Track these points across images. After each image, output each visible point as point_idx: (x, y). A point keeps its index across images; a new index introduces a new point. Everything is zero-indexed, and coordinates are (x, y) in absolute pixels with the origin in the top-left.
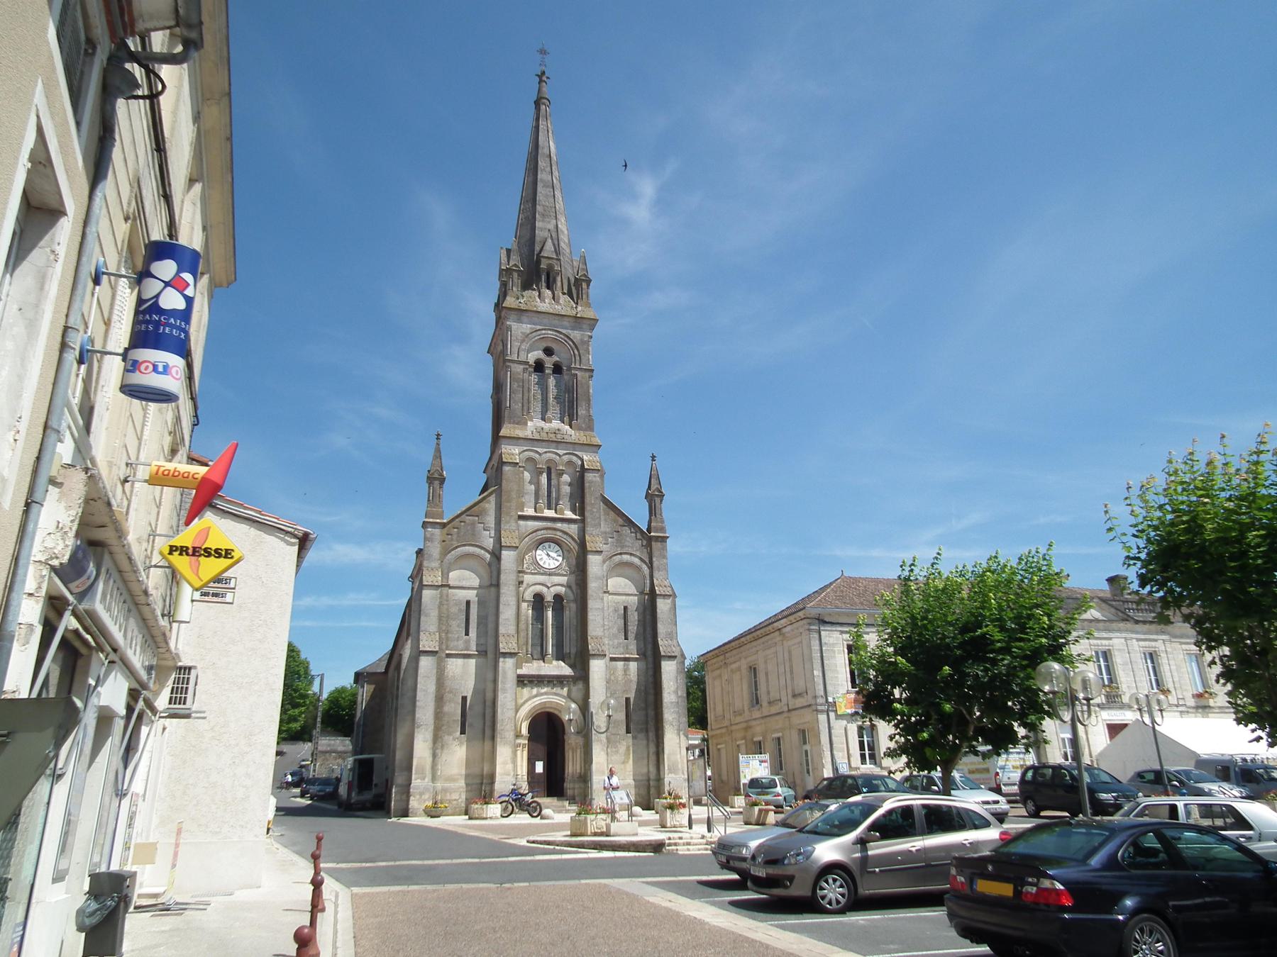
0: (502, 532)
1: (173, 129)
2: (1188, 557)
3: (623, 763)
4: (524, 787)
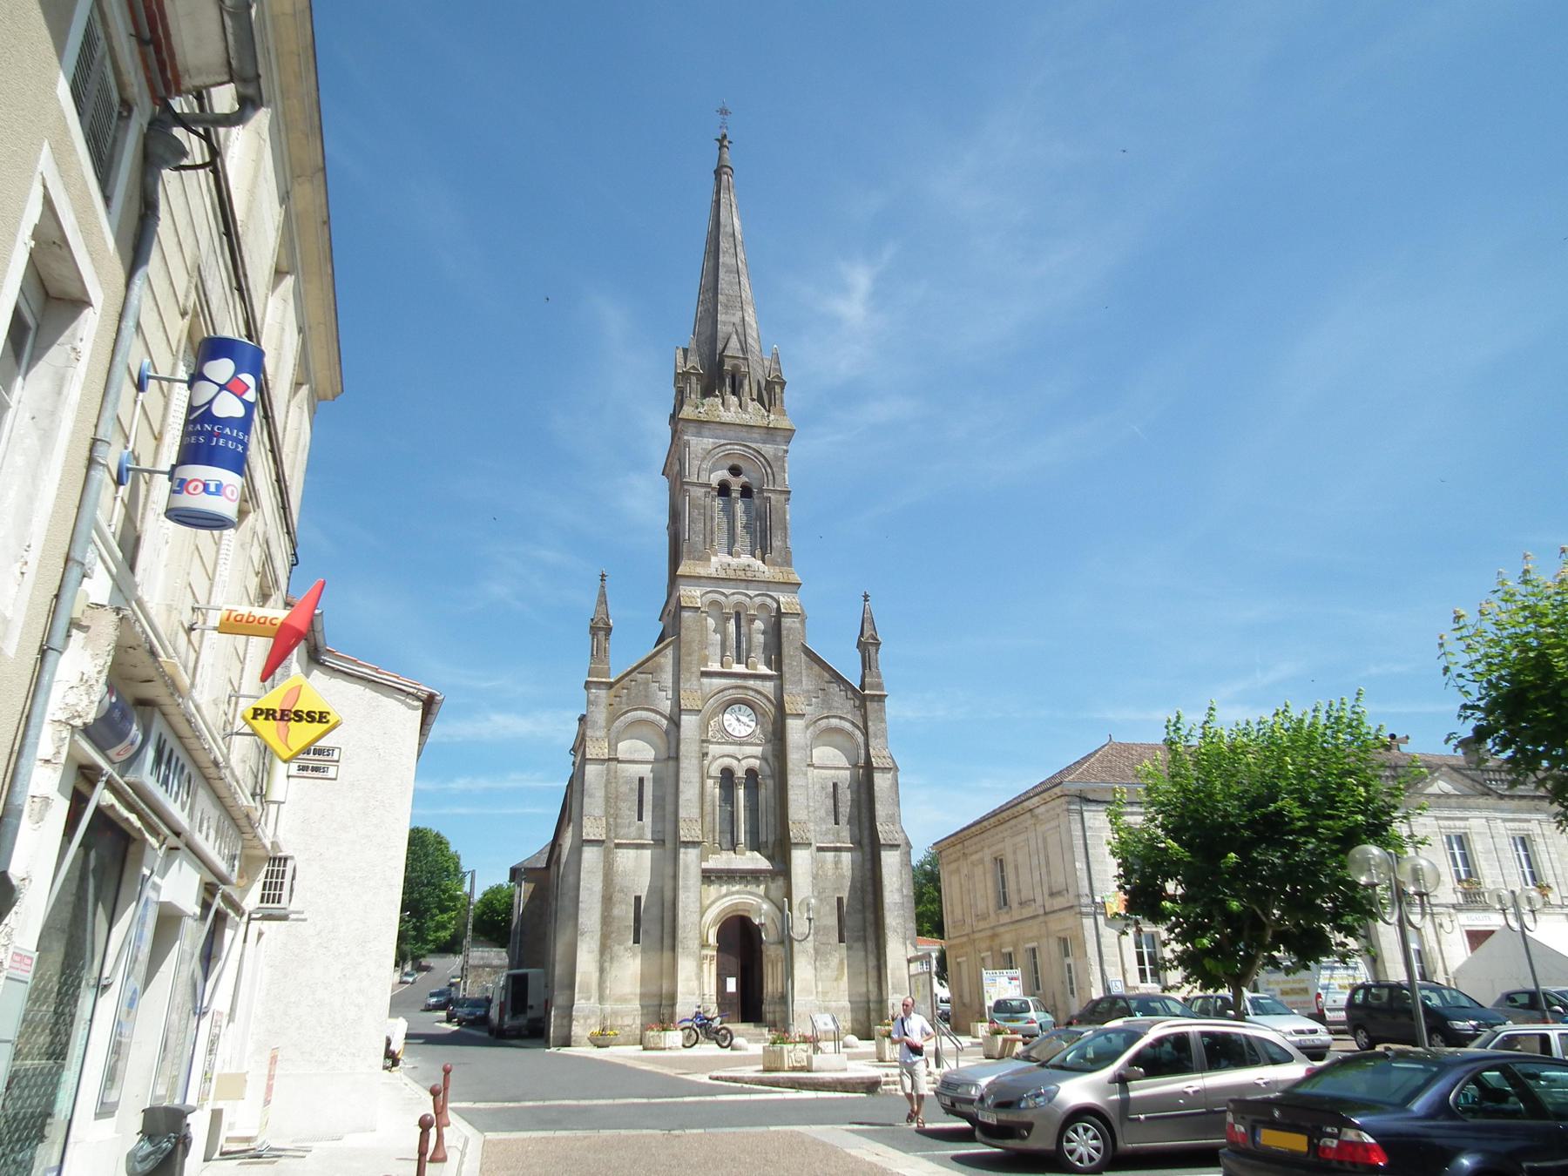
0: (682, 692)
1: (249, 210)
2: (1534, 704)
3: (836, 979)
4: (713, 1010)
